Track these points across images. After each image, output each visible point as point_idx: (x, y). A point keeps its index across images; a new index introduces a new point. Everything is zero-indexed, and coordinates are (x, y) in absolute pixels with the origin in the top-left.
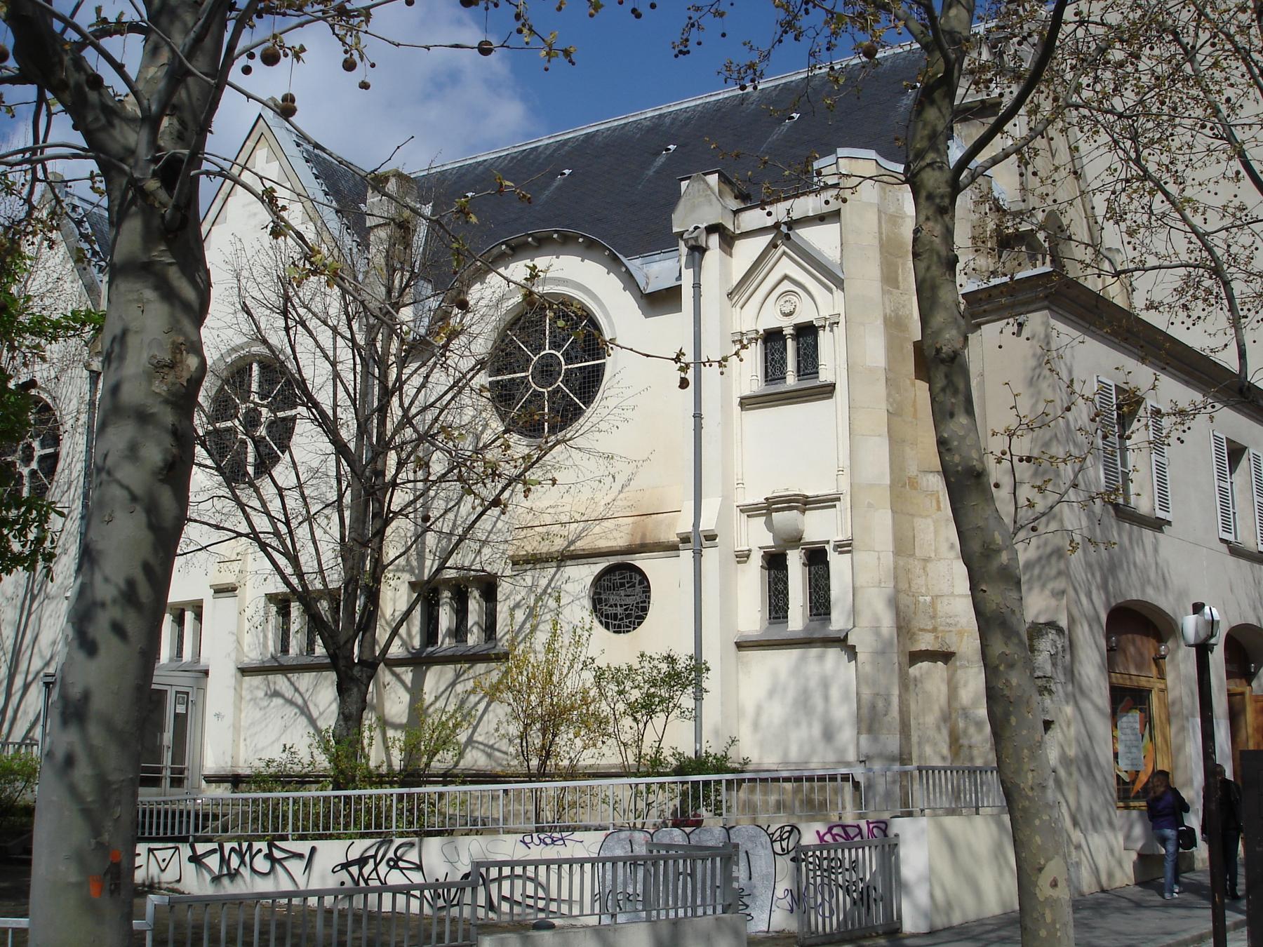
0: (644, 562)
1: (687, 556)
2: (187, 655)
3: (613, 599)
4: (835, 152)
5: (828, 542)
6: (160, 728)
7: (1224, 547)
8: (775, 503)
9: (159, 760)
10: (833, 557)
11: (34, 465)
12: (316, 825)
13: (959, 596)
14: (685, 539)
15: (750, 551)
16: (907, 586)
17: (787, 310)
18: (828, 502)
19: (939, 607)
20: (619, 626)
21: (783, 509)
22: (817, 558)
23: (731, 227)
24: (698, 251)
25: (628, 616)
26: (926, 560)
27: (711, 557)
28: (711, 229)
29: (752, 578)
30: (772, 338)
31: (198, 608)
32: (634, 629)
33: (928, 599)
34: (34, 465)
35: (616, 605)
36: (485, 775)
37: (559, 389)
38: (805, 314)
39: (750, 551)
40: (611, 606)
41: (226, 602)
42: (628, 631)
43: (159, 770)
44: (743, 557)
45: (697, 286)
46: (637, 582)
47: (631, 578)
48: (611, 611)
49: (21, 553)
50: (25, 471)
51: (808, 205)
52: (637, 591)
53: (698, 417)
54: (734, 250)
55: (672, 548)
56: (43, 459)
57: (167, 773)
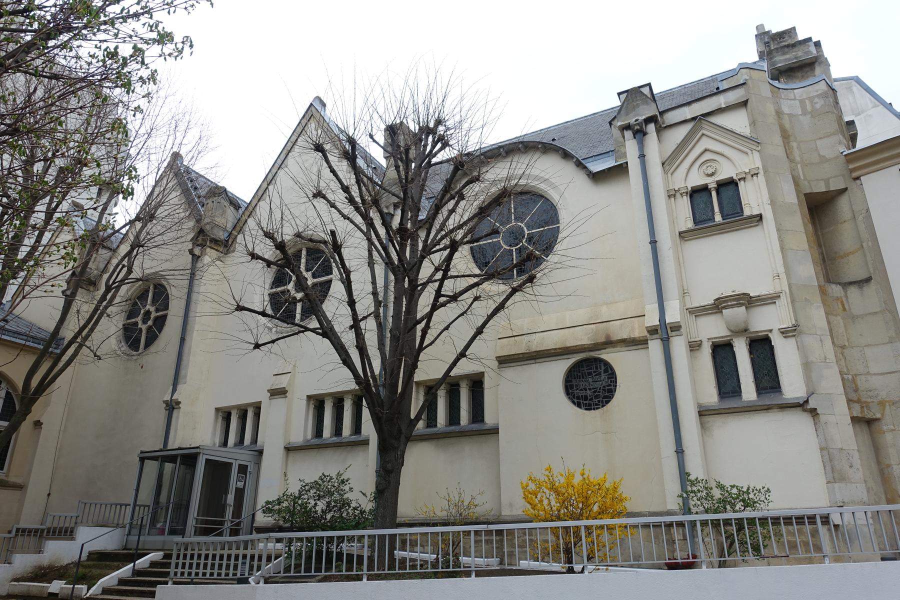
0: (612, 357)
1: (655, 346)
3: (582, 384)
5: (771, 331)
6: (226, 493)
8: (724, 302)
9: (223, 517)
10: (777, 341)
11: (150, 323)
12: (298, 566)
13: (875, 374)
14: (653, 331)
17: (710, 171)
18: (770, 299)
19: (859, 383)
20: (590, 405)
21: (732, 306)
25: (596, 397)
30: (698, 193)
32: (603, 406)
33: (850, 377)
35: (585, 389)
38: (725, 173)
40: (581, 390)
41: (279, 402)
42: (597, 408)
43: (222, 523)
45: (642, 156)
46: (602, 371)
47: (597, 368)
48: (583, 393)
50: (144, 327)
52: (603, 377)
53: (653, 242)
56: (156, 319)
57: (228, 525)
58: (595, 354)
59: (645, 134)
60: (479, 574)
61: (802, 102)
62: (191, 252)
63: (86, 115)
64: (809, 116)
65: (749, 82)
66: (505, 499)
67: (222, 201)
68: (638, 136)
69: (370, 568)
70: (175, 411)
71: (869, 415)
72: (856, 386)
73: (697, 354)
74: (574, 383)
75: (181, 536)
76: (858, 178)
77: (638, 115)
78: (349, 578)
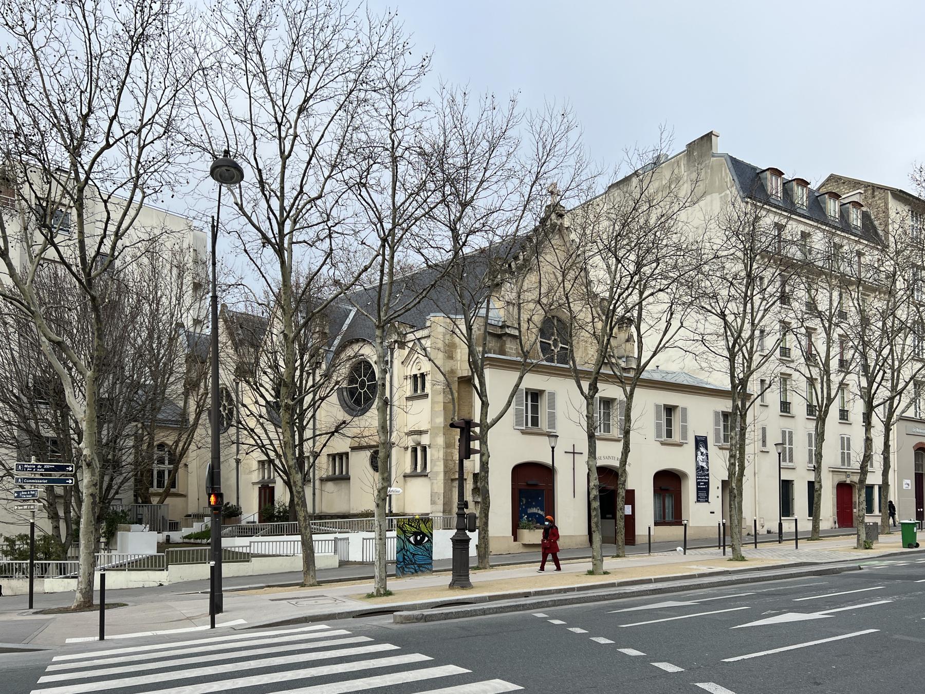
2: (344, 473)
18: (426, 432)
22: (424, 449)
31: (347, 454)
34: (226, 412)
44: (406, 449)
51: (424, 333)
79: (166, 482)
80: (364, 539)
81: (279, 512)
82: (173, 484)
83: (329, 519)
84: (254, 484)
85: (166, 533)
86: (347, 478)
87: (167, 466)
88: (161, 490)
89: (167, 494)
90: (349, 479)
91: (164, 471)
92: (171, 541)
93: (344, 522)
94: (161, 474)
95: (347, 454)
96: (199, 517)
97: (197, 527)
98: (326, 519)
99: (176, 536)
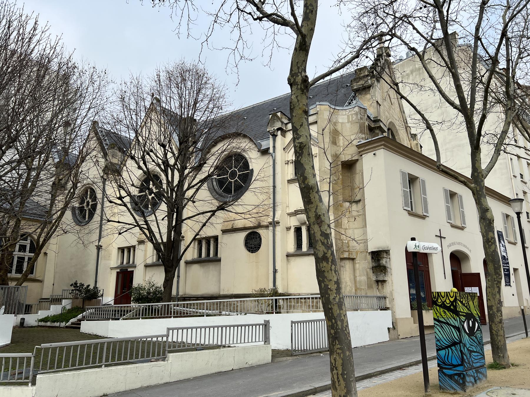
3: (251, 242)
4: (315, 104)
7: (449, 225)
8: (298, 212)
15: (291, 227)
16: (339, 237)
19: (350, 244)
20: (253, 251)
21: (300, 214)
23: (284, 129)
24: (275, 136)
25: (255, 247)
26: (346, 229)
27: (278, 229)
28: (279, 129)
29: (291, 235)
31: (216, 238)
33: (347, 241)
34: (90, 207)
36: (215, 297)
37: (236, 180)
39: (291, 227)
44: (288, 229)
48: (251, 246)
49: (393, 329)
54: (286, 136)
55: (267, 227)
56: (92, 205)
58: (255, 230)
59: (277, 136)
60: (207, 316)
61: (348, 116)
62: (102, 177)
63: (41, 176)
64: (350, 123)
65: (319, 113)
66: (222, 287)
67: (115, 151)
68: (274, 137)
69: (142, 315)
70: (100, 250)
71: (351, 257)
72: (349, 245)
73: (289, 232)
74: (248, 242)
75: (342, 268)
76: (361, 155)
77: (274, 127)
78: (167, 317)
79: (25, 269)
80: (292, 322)
81: (149, 293)
82: (31, 270)
83: (193, 300)
84: (112, 269)
85: (21, 316)
86: (217, 260)
87: (27, 254)
88: (19, 276)
89: (25, 279)
90: (219, 260)
91: (23, 259)
92: (25, 325)
93: (213, 303)
94: (21, 260)
95: (134, 247)
96: (57, 301)
97: (55, 310)
98: (190, 300)
99: (31, 319)
